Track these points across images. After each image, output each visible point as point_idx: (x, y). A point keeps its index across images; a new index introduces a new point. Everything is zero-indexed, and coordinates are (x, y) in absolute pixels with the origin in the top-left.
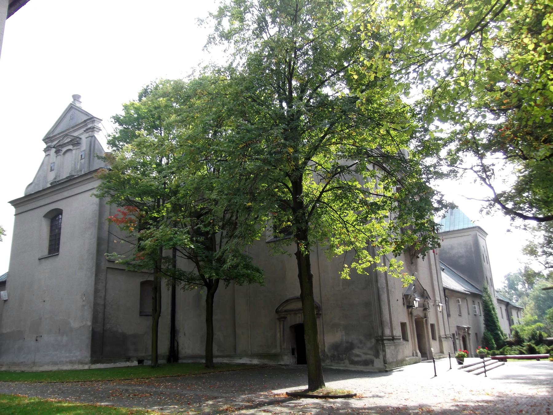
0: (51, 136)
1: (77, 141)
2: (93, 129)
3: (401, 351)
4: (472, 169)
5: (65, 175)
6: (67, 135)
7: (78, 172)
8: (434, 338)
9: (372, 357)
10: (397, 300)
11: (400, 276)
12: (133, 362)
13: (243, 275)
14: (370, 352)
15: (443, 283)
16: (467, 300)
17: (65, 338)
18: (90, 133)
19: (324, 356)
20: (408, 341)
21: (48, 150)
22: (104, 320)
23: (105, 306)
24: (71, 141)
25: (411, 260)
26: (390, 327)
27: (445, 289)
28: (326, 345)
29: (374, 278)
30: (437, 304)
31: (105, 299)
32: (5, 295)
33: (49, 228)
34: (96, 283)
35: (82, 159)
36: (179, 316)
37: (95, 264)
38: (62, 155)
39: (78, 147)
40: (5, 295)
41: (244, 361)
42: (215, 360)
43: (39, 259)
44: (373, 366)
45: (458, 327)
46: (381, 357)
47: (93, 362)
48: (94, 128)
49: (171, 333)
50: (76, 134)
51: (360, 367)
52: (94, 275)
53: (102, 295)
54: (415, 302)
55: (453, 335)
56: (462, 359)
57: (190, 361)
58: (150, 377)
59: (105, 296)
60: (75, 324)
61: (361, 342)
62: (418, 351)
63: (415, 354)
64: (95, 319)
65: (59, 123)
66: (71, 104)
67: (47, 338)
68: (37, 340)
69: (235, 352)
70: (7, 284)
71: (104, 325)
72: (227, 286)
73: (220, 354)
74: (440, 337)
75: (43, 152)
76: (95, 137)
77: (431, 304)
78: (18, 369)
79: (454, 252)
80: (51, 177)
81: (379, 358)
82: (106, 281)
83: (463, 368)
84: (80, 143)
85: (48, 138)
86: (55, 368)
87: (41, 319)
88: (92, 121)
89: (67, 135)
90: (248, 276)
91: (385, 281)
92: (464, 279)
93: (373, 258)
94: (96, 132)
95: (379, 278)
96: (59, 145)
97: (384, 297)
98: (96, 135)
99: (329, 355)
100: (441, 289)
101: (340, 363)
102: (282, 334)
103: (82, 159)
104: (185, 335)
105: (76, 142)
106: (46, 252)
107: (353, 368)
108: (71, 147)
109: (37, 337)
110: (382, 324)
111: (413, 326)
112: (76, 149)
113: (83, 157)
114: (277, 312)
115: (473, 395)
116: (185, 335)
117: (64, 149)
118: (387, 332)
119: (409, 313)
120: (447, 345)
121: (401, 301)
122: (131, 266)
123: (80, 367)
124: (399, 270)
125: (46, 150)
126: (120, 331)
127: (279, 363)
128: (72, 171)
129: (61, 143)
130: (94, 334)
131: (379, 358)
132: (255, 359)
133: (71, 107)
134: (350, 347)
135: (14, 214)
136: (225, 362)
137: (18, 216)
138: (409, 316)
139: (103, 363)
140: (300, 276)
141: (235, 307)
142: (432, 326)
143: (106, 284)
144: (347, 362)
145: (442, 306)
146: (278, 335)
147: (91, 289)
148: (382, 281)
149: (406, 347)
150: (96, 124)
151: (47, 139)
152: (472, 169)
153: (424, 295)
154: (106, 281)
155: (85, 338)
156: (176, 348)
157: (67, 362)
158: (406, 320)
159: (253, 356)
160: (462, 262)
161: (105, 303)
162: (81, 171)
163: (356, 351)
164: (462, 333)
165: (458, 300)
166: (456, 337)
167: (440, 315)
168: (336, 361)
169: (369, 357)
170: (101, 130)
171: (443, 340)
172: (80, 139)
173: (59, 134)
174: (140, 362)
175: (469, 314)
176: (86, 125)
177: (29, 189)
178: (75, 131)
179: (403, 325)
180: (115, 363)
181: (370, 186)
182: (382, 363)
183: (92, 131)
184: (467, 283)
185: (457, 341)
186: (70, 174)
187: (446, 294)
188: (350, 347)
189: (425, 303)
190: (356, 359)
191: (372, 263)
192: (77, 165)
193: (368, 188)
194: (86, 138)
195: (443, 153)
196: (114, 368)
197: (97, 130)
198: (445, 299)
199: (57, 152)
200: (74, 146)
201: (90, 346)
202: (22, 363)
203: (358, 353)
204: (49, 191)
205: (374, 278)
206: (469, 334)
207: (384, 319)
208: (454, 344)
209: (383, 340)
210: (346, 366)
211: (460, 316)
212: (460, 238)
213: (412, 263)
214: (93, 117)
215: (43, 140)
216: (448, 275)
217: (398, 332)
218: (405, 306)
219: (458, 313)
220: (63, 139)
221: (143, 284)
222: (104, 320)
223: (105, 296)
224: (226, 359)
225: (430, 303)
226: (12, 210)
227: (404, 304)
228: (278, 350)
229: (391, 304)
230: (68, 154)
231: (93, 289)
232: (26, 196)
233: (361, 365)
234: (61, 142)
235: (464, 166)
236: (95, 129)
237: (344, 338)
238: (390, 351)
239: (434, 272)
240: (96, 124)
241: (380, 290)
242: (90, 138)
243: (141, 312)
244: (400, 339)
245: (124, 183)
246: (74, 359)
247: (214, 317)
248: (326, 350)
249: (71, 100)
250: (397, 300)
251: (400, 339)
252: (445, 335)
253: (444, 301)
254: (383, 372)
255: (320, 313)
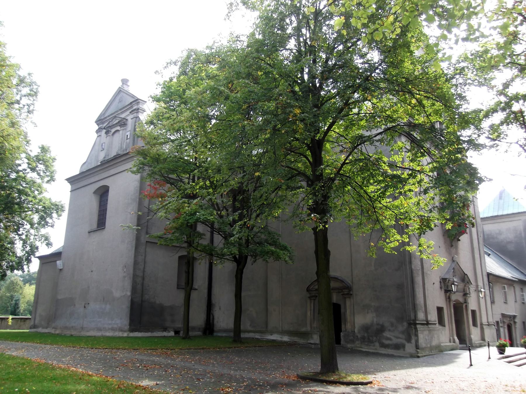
0: (102, 118)
1: (124, 122)
2: (137, 110)
3: (436, 336)
4: (517, 143)
5: (113, 154)
6: (115, 117)
7: (123, 151)
8: (475, 325)
9: (404, 341)
10: (434, 284)
11: (430, 257)
12: (170, 332)
13: (268, 253)
14: (401, 336)
15: (487, 268)
16: (514, 287)
17: (108, 307)
18: (135, 114)
19: (353, 337)
20: (445, 326)
21: (100, 131)
22: (143, 291)
23: (143, 279)
24: (119, 122)
25: (451, 242)
26: (424, 310)
27: (489, 275)
28: (357, 326)
29: (407, 259)
30: (479, 289)
31: (144, 271)
32: (60, 264)
33: (98, 203)
34: (135, 256)
35: (127, 139)
36: (216, 290)
37: (135, 238)
38: (111, 136)
39: (125, 128)
40: (60, 264)
41: (275, 337)
42: (243, 335)
43: (89, 232)
44: (404, 350)
45: (503, 315)
46: (413, 341)
47: (132, 330)
48: (138, 109)
49: (207, 307)
50: (123, 116)
51: (390, 351)
52: (134, 248)
53: (142, 267)
54: (453, 286)
55: (497, 322)
56: (503, 348)
57: (224, 335)
58: (175, 348)
59: (144, 268)
60: (117, 294)
61: (392, 325)
62: (456, 338)
63: (452, 341)
64: (134, 290)
65: (109, 106)
66: (120, 87)
67: (94, 306)
68: (85, 307)
69: (267, 327)
70: (63, 255)
71: (142, 296)
72: (254, 262)
73: (252, 329)
74: (482, 324)
75: (96, 133)
76: (139, 118)
77: (472, 288)
78: (68, 333)
79: (502, 237)
80: (102, 156)
81: (411, 343)
82: (145, 254)
83: (503, 358)
84: (126, 124)
85: (100, 120)
86: (99, 334)
87: (89, 287)
88: (137, 103)
89: (115, 117)
90: (273, 253)
91: (420, 263)
92: (513, 266)
93: (402, 236)
94: (140, 114)
95: (413, 259)
96: (109, 127)
97: (418, 279)
98: (140, 116)
99: (359, 336)
100: (485, 274)
101: (370, 346)
102: (312, 313)
103: (127, 139)
104: (220, 309)
105: (123, 123)
106: (95, 226)
107: (383, 351)
108: (118, 128)
109: (85, 304)
110: (415, 306)
111: (451, 311)
112: (123, 130)
113: (128, 138)
114: (308, 290)
115: (507, 391)
116: (220, 309)
117: (113, 130)
118: (421, 316)
119: (447, 297)
120: (490, 333)
121: (438, 285)
122: (162, 240)
123: (120, 334)
124: (429, 251)
125: (97, 132)
126: (158, 302)
127: (309, 342)
128: (119, 150)
129: (111, 124)
130: (132, 303)
131: (411, 343)
132: (286, 337)
133: (120, 91)
134: (381, 329)
135: (70, 190)
136: (257, 337)
137: (73, 192)
138: (446, 300)
139: (141, 332)
140: (316, 252)
141: (267, 284)
142: (473, 312)
143: (145, 257)
144: (377, 344)
145: (485, 292)
146: (309, 313)
147: (131, 261)
148: (416, 264)
149: (441, 333)
150: (140, 106)
151: (99, 121)
152: (517, 143)
153: (464, 279)
154: (145, 254)
155: (125, 308)
156: (211, 321)
157: (109, 329)
158: (442, 303)
159: (283, 333)
160: (511, 247)
161: (144, 274)
162: (126, 150)
163: (387, 334)
164: (507, 321)
165: (504, 287)
166: (501, 325)
167: (482, 302)
168: (366, 343)
169: (399, 341)
170: (145, 111)
171: (484, 327)
172: (127, 120)
173: (109, 116)
174: (177, 332)
175: (516, 302)
176: (132, 107)
177: (83, 167)
178: (122, 113)
179: (440, 310)
180: (152, 332)
181: (398, 159)
182: (415, 348)
183: (137, 113)
184: (514, 269)
185: (502, 330)
186: (117, 153)
187: (490, 279)
188: (381, 329)
189: (466, 287)
190: (387, 342)
191: (401, 241)
192: (124, 144)
193: (395, 161)
194: (132, 119)
195: (486, 124)
196: (151, 337)
197: (142, 111)
198: (489, 285)
199: (107, 133)
200: (121, 127)
201: (128, 315)
202: (72, 327)
203: (388, 336)
204: (99, 169)
205: (407, 259)
206: (515, 323)
207: (417, 302)
208: (498, 331)
209: (415, 324)
210: (376, 349)
211: (506, 303)
212: (510, 223)
213: (452, 246)
214: (138, 99)
215: (96, 122)
216: (494, 260)
217: (433, 317)
218: (443, 290)
219: (503, 300)
220: (112, 121)
221: (180, 258)
222: (143, 291)
223: (144, 268)
224: (257, 334)
225: (471, 288)
226: (68, 187)
227: (441, 288)
228: (309, 328)
229: (426, 287)
230: (117, 135)
231: (133, 261)
232: (81, 173)
233: (392, 349)
234: (111, 123)
235: (509, 139)
236: (140, 110)
237: (375, 320)
238: (423, 336)
239: (477, 256)
240: (140, 106)
241: (414, 272)
242: (135, 119)
243: (178, 285)
244: (435, 324)
245: (157, 159)
246: (115, 326)
247: (243, 294)
248: (356, 331)
249: (120, 84)
250: (434, 284)
251: (435, 324)
252: (488, 322)
253: (487, 287)
254: (415, 357)
255: (351, 293)
